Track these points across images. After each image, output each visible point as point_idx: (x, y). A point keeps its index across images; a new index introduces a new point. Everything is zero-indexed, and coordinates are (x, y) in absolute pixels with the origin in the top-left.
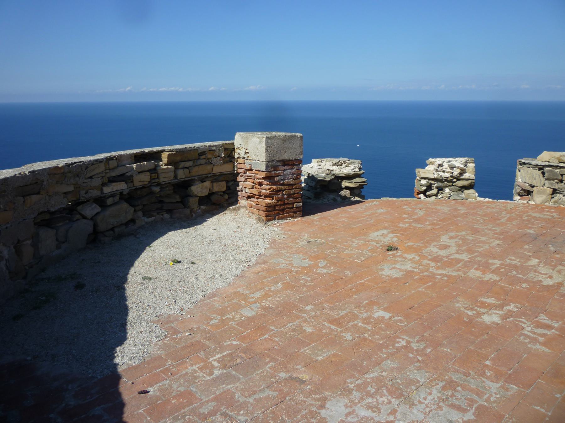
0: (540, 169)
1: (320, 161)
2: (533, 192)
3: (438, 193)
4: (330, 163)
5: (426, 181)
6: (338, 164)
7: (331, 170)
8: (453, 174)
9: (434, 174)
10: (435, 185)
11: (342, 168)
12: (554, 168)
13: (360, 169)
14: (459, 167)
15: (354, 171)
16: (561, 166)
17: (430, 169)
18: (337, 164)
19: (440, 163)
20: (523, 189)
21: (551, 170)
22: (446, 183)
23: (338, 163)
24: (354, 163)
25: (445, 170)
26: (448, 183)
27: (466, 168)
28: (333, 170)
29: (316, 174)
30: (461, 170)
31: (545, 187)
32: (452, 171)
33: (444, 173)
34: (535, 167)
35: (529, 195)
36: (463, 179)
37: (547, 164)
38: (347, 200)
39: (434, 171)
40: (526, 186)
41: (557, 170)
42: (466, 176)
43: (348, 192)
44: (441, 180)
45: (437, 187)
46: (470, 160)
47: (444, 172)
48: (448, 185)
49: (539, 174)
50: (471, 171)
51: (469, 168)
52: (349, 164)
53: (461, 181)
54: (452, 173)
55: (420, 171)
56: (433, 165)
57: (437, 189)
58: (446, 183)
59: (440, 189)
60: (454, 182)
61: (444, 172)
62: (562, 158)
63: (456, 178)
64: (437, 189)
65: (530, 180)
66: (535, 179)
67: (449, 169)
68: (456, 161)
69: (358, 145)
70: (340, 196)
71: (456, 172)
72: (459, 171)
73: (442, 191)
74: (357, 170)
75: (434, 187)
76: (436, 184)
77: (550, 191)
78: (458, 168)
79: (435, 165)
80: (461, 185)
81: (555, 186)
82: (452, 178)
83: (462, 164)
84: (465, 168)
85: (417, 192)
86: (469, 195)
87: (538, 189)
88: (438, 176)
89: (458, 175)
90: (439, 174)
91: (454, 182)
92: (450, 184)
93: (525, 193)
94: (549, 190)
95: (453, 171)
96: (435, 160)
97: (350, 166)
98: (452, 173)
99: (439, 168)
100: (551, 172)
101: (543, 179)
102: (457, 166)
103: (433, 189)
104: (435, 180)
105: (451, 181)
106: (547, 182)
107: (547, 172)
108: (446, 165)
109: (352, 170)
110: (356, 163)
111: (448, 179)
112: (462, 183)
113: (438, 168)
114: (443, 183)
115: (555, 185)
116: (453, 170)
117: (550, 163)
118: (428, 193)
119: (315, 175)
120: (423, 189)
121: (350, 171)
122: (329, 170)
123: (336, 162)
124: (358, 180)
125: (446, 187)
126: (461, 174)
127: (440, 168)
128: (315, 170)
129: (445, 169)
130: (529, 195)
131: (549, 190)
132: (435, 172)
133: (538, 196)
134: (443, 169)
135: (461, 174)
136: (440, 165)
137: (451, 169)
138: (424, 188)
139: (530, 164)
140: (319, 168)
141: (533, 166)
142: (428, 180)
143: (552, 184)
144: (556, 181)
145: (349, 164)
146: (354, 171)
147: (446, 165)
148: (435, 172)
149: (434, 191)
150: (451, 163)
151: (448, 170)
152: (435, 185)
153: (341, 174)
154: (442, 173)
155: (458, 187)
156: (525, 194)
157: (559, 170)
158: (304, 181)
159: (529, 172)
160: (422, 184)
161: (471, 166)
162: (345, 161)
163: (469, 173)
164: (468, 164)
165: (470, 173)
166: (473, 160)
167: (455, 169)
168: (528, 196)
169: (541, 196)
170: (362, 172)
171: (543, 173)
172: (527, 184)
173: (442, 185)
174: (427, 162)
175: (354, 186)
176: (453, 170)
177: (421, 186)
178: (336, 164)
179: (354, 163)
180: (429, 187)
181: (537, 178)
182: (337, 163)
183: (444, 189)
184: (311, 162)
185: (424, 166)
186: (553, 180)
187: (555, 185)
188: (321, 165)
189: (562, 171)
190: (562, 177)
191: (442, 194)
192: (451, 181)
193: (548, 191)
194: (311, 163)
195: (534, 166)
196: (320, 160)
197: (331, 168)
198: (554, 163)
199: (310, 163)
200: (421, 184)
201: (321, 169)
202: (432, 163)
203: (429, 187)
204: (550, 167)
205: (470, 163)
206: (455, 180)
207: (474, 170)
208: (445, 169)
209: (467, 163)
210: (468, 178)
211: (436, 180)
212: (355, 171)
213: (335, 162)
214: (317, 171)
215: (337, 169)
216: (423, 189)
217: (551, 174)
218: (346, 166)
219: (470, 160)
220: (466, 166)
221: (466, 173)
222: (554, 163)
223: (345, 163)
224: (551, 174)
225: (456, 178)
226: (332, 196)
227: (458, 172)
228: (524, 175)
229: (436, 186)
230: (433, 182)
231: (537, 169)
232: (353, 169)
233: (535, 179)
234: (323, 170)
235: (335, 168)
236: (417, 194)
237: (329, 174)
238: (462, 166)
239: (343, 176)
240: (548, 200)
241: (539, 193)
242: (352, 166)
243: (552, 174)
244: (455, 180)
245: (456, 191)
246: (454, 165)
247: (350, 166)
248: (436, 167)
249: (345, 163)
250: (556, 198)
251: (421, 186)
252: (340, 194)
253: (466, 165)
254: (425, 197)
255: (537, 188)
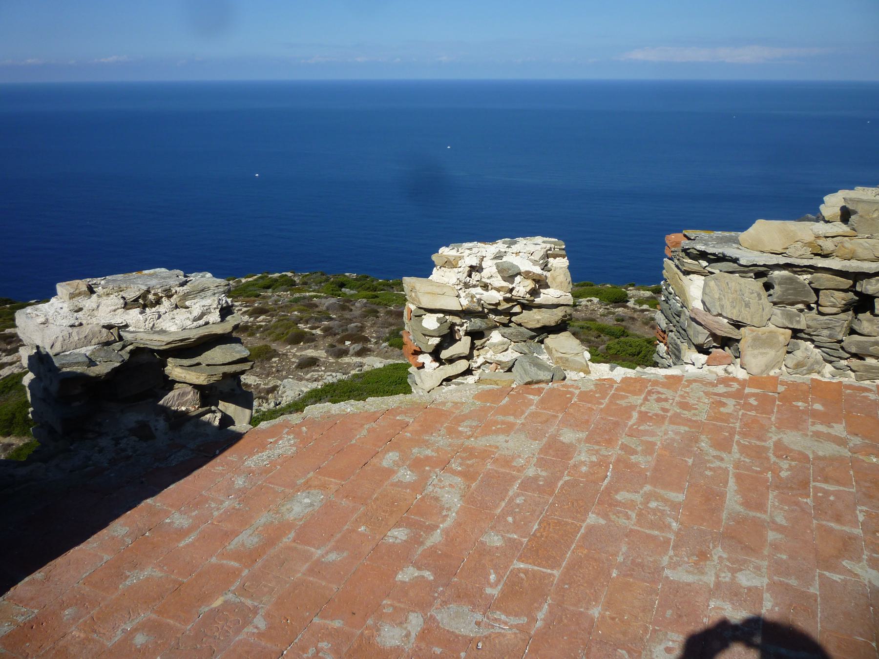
0: (758, 275)
1: (84, 288)
2: (741, 342)
3: (473, 347)
4: (115, 301)
5: (438, 319)
6: (143, 302)
7: (120, 328)
8: (514, 293)
9: (458, 296)
10: (464, 328)
11: (160, 317)
12: (795, 272)
13: (226, 312)
14: (530, 272)
15: (201, 322)
16: (819, 266)
17: (445, 280)
18: (141, 301)
19: (474, 264)
20: (714, 335)
21: (790, 279)
22: (492, 316)
23: (144, 296)
24: (203, 290)
25: (488, 281)
26: (497, 318)
27: (548, 274)
28: (127, 326)
29: (57, 348)
30: (534, 280)
31: (771, 327)
32: (511, 286)
33: (487, 290)
34: (745, 270)
35: (727, 348)
36: (540, 306)
37: (782, 260)
38: (188, 428)
39: (459, 287)
40: (722, 325)
41: (805, 278)
42: (547, 296)
43: (189, 396)
44: (480, 312)
45: (467, 333)
46: (554, 248)
47: (486, 287)
48: (498, 322)
49: (757, 290)
50: (561, 283)
51: (555, 274)
52: (186, 297)
53: (535, 310)
54: (511, 290)
55: (417, 288)
56: (456, 270)
57: (469, 338)
58: (494, 316)
59: (476, 335)
60: (516, 314)
61: (486, 287)
62: (820, 242)
63: (519, 303)
64: (469, 338)
65: (734, 307)
66: (747, 305)
67: (500, 278)
68: (517, 254)
69: (257, 175)
70: (165, 410)
71: (522, 288)
72: (530, 285)
73: (484, 340)
74: (215, 317)
75: (462, 333)
76: (465, 325)
77: (785, 338)
78: (527, 275)
79: (460, 270)
80: (538, 326)
81: (798, 322)
82: (511, 304)
83: (535, 262)
84: (545, 273)
85: (414, 350)
86: (567, 360)
87: (754, 334)
88: (472, 301)
89: (528, 296)
90: (473, 297)
91: (516, 314)
92: (505, 319)
93: (715, 342)
94: (783, 334)
95: (514, 285)
96: (458, 254)
97: (187, 303)
98: (511, 290)
99: (470, 276)
100: (791, 284)
101: (766, 301)
102: (523, 269)
103: (460, 340)
104: (462, 315)
105: (508, 313)
106: (777, 310)
107: (780, 284)
108: (490, 267)
109: (195, 320)
110: (209, 293)
111: (499, 308)
112: (539, 317)
113: (468, 279)
114: (486, 320)
115: (798, 319)
116: (512, 283)
117: (790, 257)
118: (445, 354)
119: (56, 355)
120: (430, 343)
121: (188, 323)
122: (109, 327)
123: (138, 294)
124: (218, 354)
125: (495, 327)
126: (534, 293)
127: (476, 276)
128: (54, 337)
129: (488, 278)
130: (727, 348)
131: (783, 334)
132: (461, 289)
133: (756, 352)
134: (483, 280)
135: (534, 293)
136: (474, 269)
137: (509, 279)
138: (436, 341)
139: (735, 261)
140: (72, 322)
141: (742, 269)
142: (442, 315)
143: (790, 317)
144: (801, 306)
145: (186, 297)
146: (201, 322)
147: (490, 267)
148: (461, 289)
149: (462, 346)
150: (504, 259)
151: (498, 282)
152: (464, 328)
153: (157, 342)
154: (479, 290)
155: (528, 329)
156: (715, 344)
157: (809, 276)
158: (29, 365)
159: (733, 285)
160: (426, 329)
161: (560, 265)
162: (169, 290)
163: (557, 287)
164: (551, 260)
165: (560, 286)
166: (564, 247)
167: (518, 279)
168: (723, 349)
169: (761, 351)
170: (232, 321)
171: (768, 286)
172: (726, 321)
173: (484, 326)
174: (434, 257)
175: (205, 383)
176: (512, 283)
177: (425, 335)
178: (136, 300)
179: (203, 290)
180: (449, 338)
181: (754, 301)
182: (139, 297)
183: (486, 333)
184: (54, 293)
185: (424, 270)
186: (793, 304)
187: (798, 319)
188: (81, 309)
189: (818, 279)
190: (818, 296)
191: (483, 347)
192: (508, 313)
193: (781, 338)
194: (53, 300)
195: (746, 269)
196: (82, 285)
197: (119, 319)
198: (801, 257)
199: (48, 301)
200: (424, 332)
201: (81, 324)
202: (450, 264)
203: (449, 338)
204: (784, 269)
205: (555, 256)
206: (517, 309)
207: (569, 279)
208: (488, 278)
209: (548, 256)
210: (555, 301)
211: (465, 313)
212: (207, 323)
213: (131, 295)
214: (61, 339)
215: (138, 321)
216: (430, 343)
217: (788, 289)
218: (177, 307)
219: (554, 248)
220: (545, 267)
221: (547, 286)
222: (801, 257)
223: (169, 297)
224: (788, 289)
225: (519, 303)
226: (132, 418)
227: (528, 289)
228: (717, 296)
229: (466, 330)
230: (457, 320)
231: (751, 277)
232: (200, 317)
233: (747, 305)
234: (86, 330)
235: (133, 316)
236: (413, 354)
237: (115, 341)
238: (537, 270)
239: (161, 348)
240: (779, 359)
241: (760, 342)
242: (197, 306)
243: (795, 289)
244: (517, 309)
245: (525, 341)
246: (513, 266)
247: (187, 303)
248: (463, 277)
249: (169, 297)
250: (799, 355)
251: (425, 335)
252: (162, 406)
253: (546, 265)
254: (438, 364)
255: (753, 331)
